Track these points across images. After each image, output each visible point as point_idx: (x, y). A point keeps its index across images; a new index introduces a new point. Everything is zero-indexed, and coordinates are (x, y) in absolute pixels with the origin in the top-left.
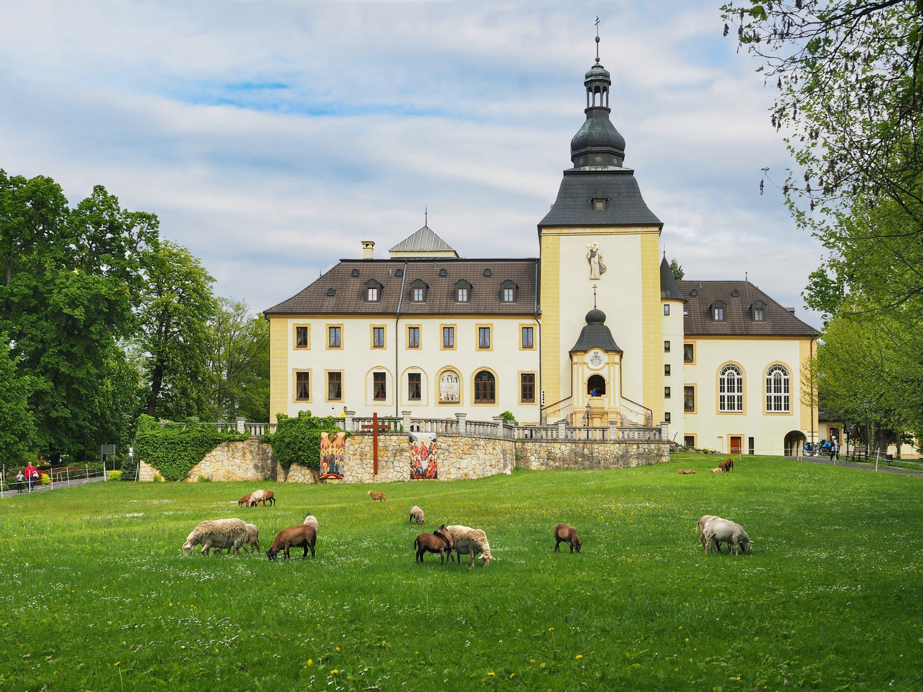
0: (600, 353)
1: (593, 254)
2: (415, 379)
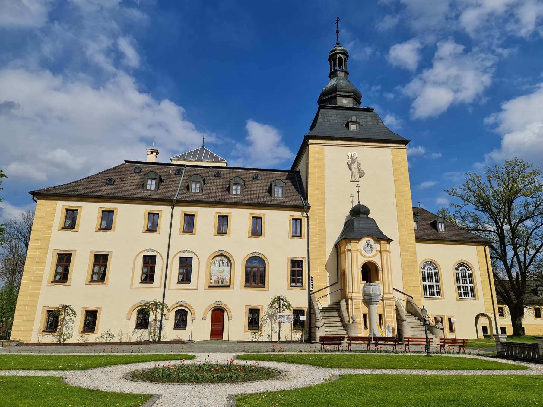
0: (372, 242)
1: (353, 160)
2: (186, 264)
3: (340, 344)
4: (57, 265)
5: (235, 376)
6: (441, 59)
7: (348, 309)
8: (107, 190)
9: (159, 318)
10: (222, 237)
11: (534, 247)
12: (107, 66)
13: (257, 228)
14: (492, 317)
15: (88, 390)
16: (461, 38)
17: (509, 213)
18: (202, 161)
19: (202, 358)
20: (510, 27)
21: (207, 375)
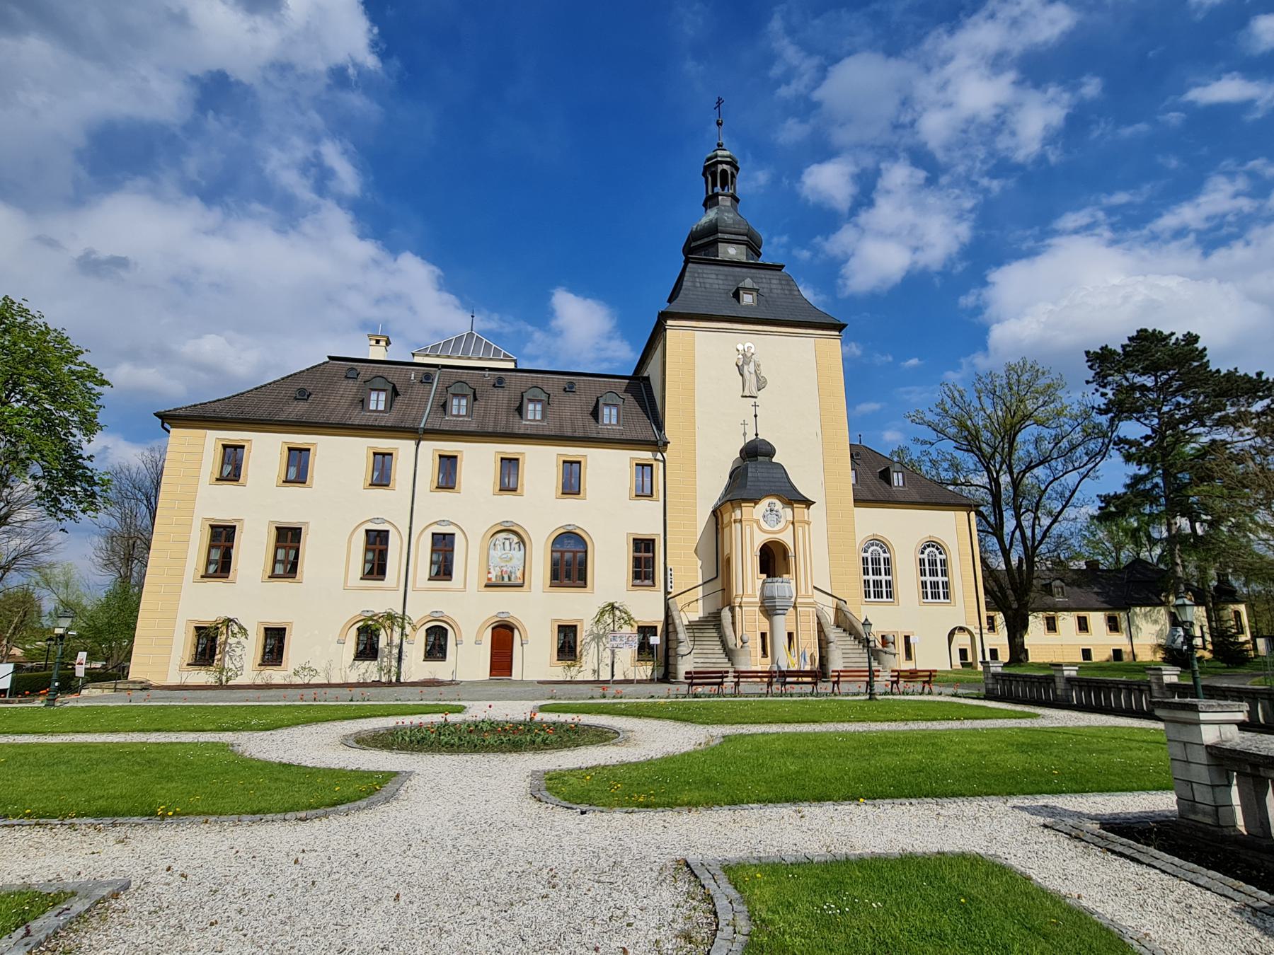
0: (778, 505)
1: (747, 358)
2: (443, 545)
3: (722, 683)
4: (211, 547)
5: (539, 739)
6: (888, 192)
7: (734, 623)
8: (295, 410)
9: (396, 641)
10: (508, 498)
11: (1050, 513)
12: (302, 190)
13: (572, 483)
14: (976, 632)
15: (280, 764)
16: (920, 157)
17: (1010, 454)
18: (469, 358)
19: (477, 711)
20: (1003, 142)
21: (490, 738)
